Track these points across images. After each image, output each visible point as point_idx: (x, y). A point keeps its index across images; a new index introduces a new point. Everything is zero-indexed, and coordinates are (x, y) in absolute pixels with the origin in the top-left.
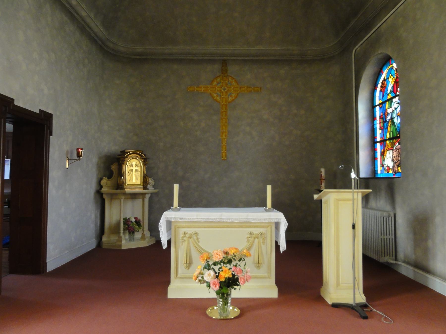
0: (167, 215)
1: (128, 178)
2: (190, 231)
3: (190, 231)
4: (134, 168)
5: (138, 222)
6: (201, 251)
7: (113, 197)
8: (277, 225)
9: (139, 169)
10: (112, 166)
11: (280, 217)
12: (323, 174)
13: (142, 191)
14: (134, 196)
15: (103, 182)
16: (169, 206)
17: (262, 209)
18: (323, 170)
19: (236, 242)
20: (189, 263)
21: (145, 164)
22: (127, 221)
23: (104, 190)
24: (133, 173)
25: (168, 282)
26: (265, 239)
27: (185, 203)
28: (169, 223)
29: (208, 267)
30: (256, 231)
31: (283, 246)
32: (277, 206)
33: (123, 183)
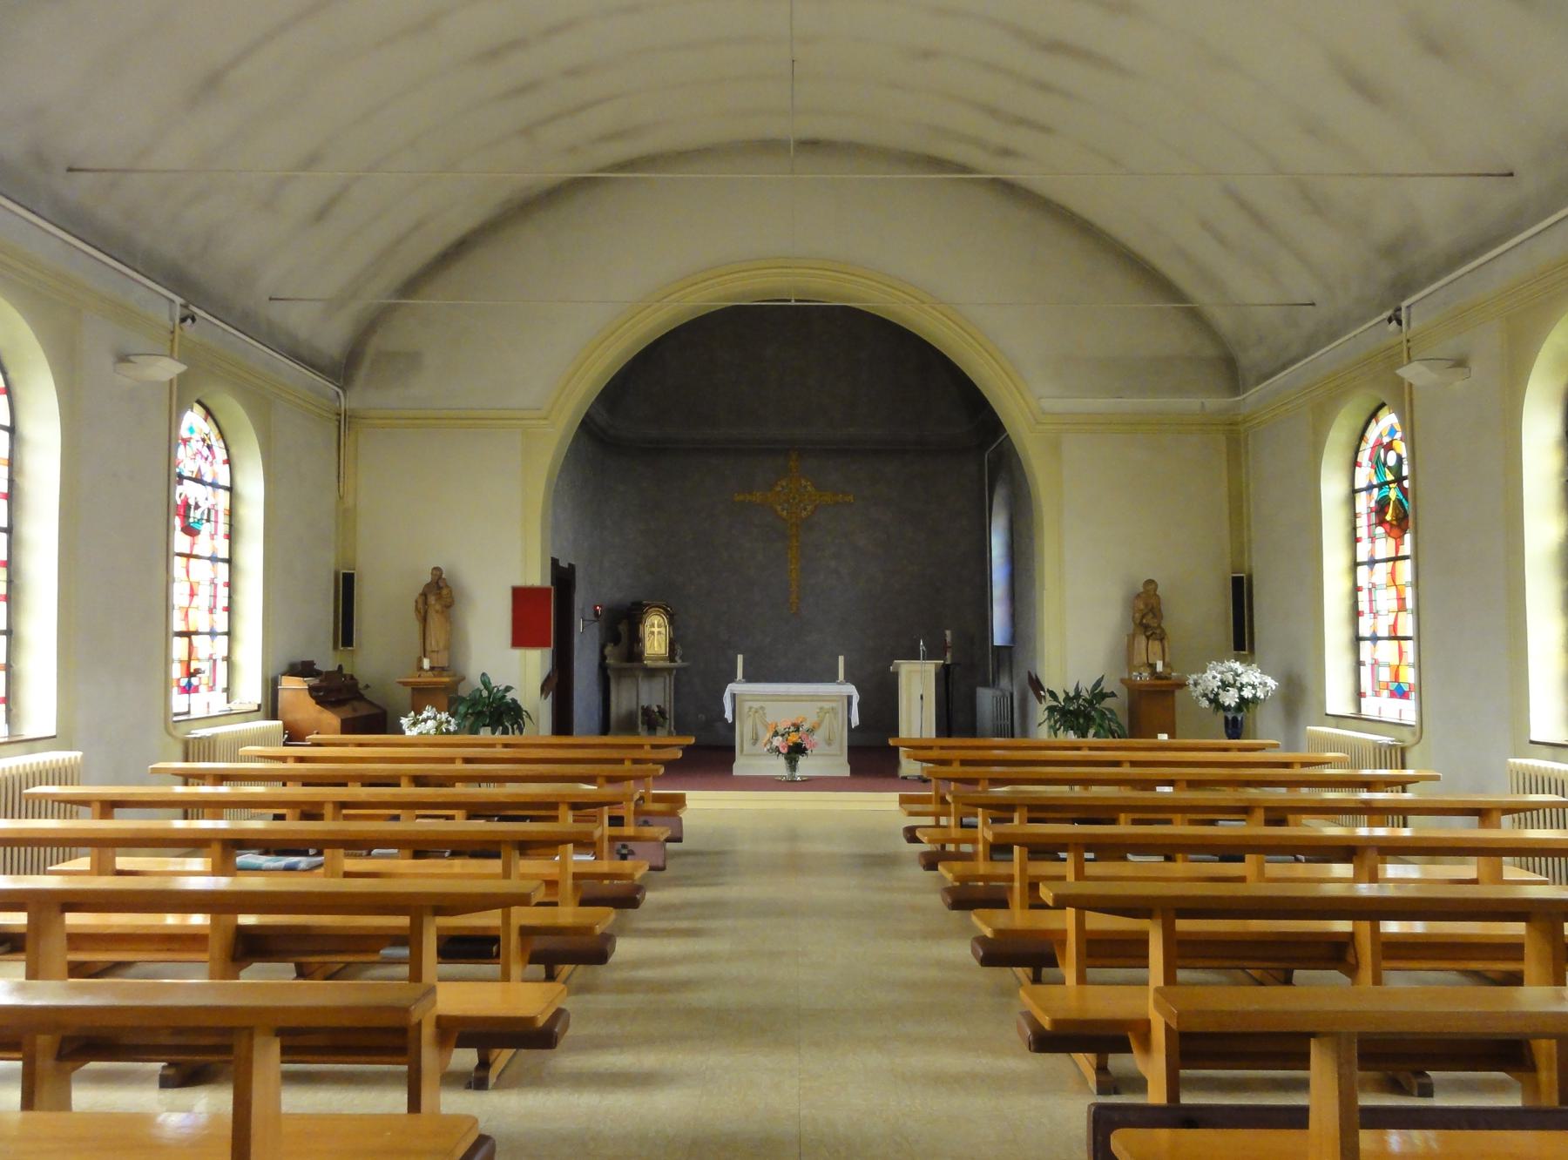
0: (731, 688)
1: (647, 644)
2: (756, 705)
3: (756, 705)
4: (656, 630)
5: (662, 712)
6: (766, 726)
7: (621, 673)
8: (850, 698)
9: (663, 630)
10: (622, 627)
11: (851, 690)
12: (948, 639)
13: (668, 664)
14: (652, 673)
15: (609, 650)
16: (732, 678)
17: (891, 781)
18: (948, 633)
19: (807, 714)
20: (755, 740)
21: (671, 623)
22: (646, 711)
23: (610, 661)
24: (656, 636)
25: (733, 760)
26: (836, 714)
27: (750, 678)
28: (734, 696)
29: (776, 734)
30: (827, 705)
31: (855, 721)
32: (849, 678)
33: (641, 653)
